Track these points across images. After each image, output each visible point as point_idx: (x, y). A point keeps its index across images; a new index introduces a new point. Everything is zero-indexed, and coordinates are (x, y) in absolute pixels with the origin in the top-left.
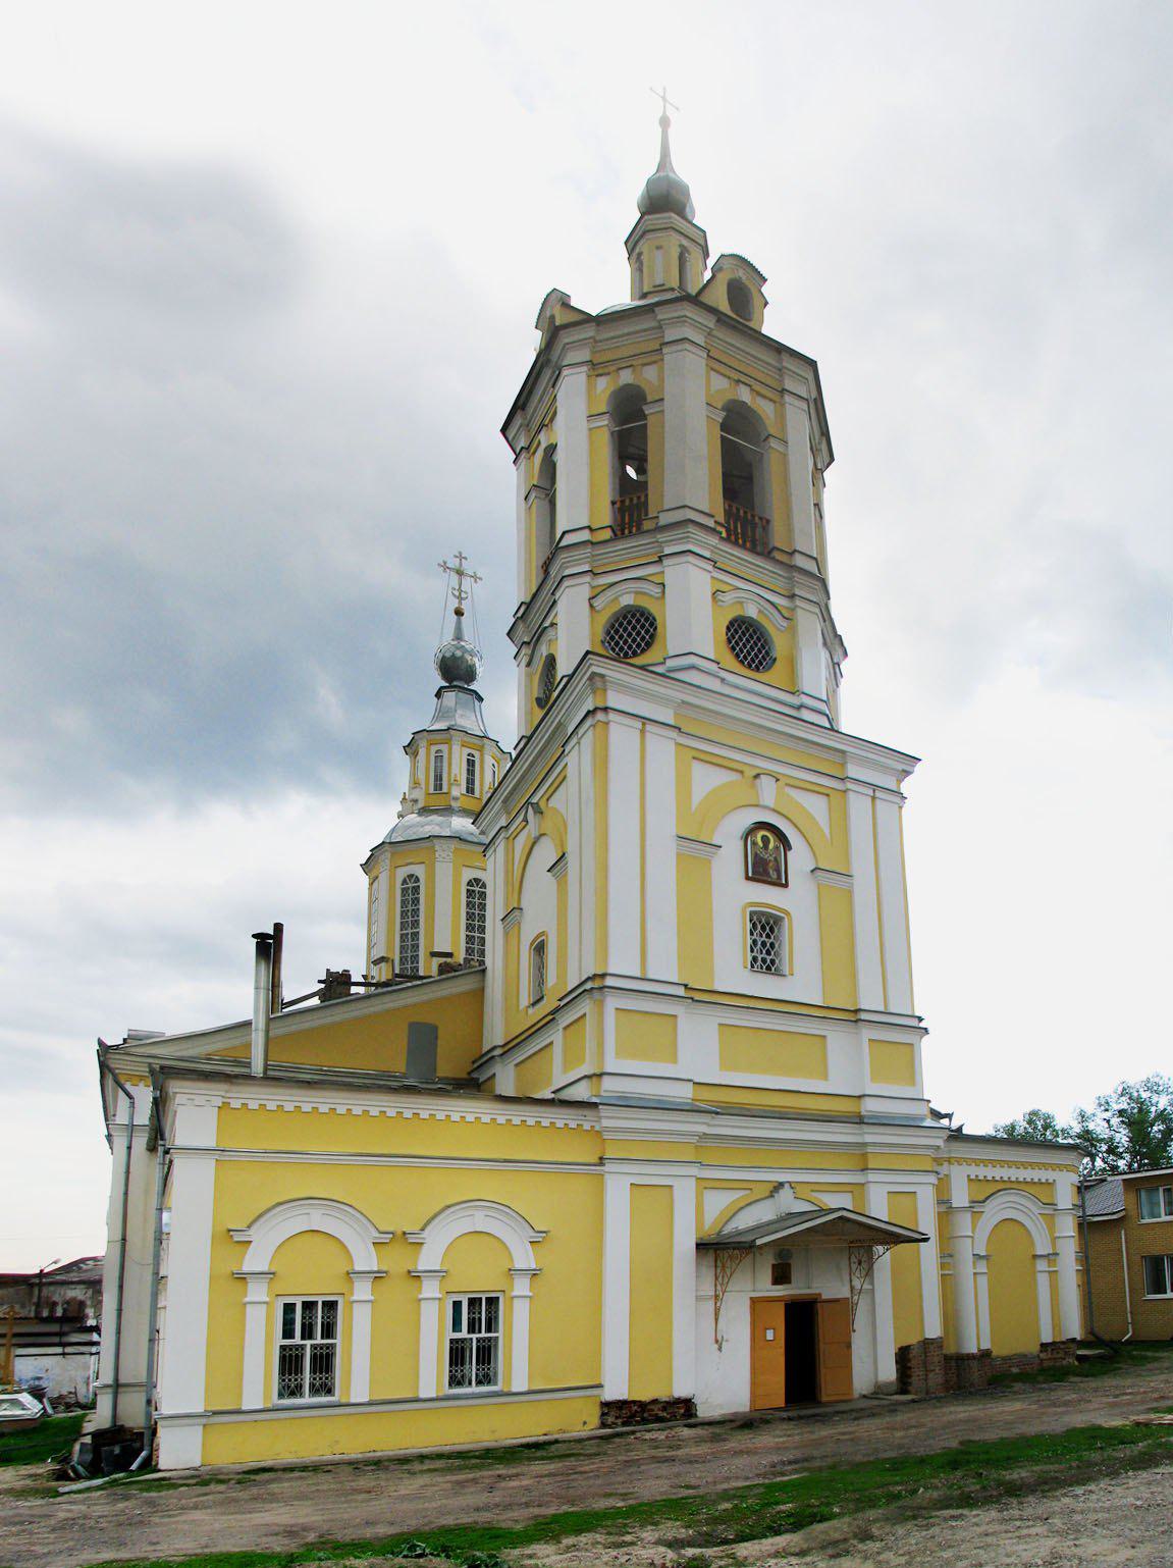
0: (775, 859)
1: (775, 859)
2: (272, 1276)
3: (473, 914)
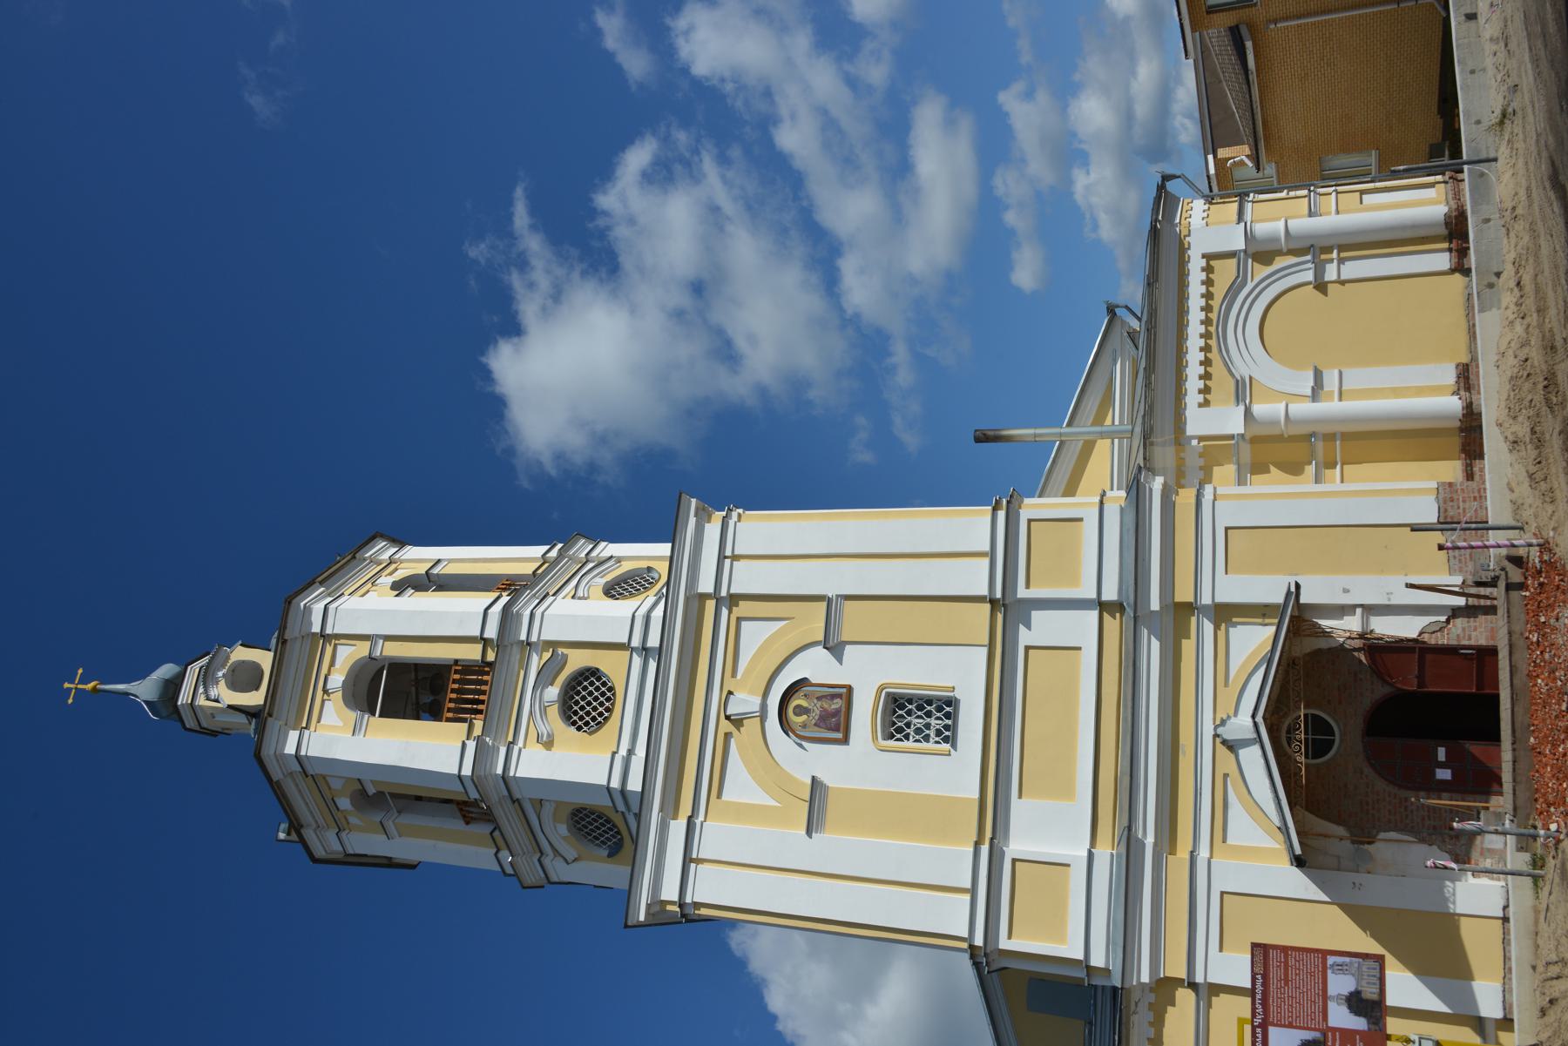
0: (819, 698)
1: (819, 698)
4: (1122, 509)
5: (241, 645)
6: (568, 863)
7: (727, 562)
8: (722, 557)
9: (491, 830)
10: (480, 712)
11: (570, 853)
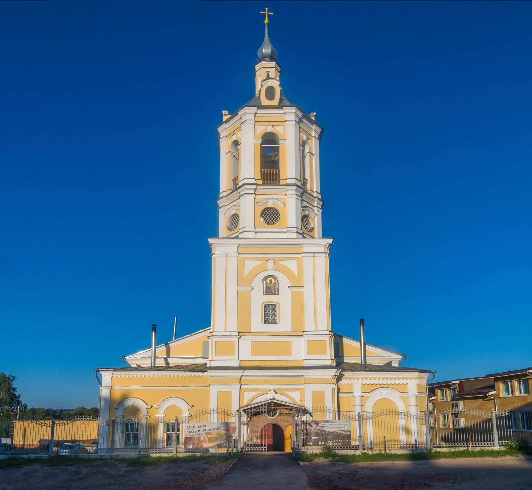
4: (386, 379)
5: (281, 90)
6: (224, 214)
7: (312, 255)
8: (314, 253)
9: (231, 189)
10: (264, 182)
11: (227, 215)
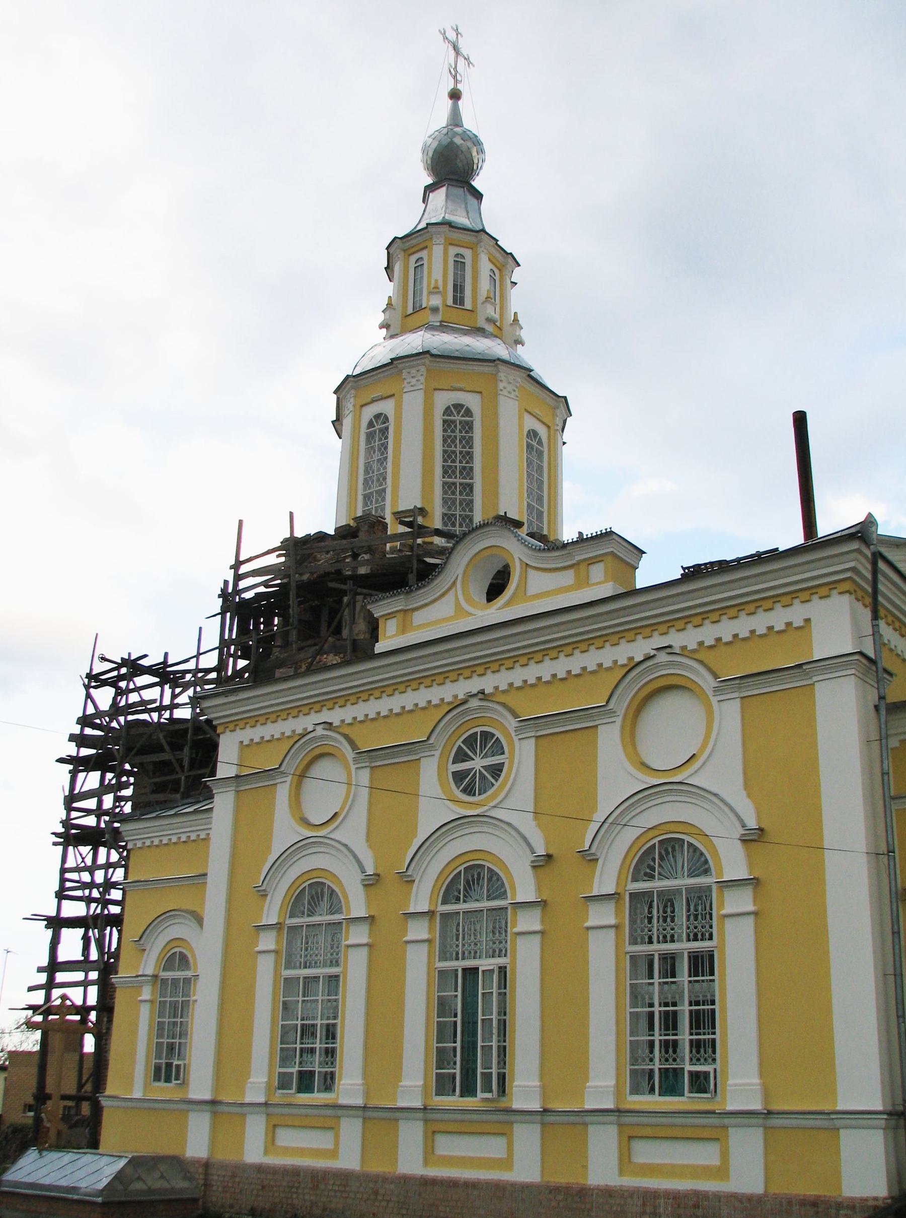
2: (279, 926)
3: (454, 452)
